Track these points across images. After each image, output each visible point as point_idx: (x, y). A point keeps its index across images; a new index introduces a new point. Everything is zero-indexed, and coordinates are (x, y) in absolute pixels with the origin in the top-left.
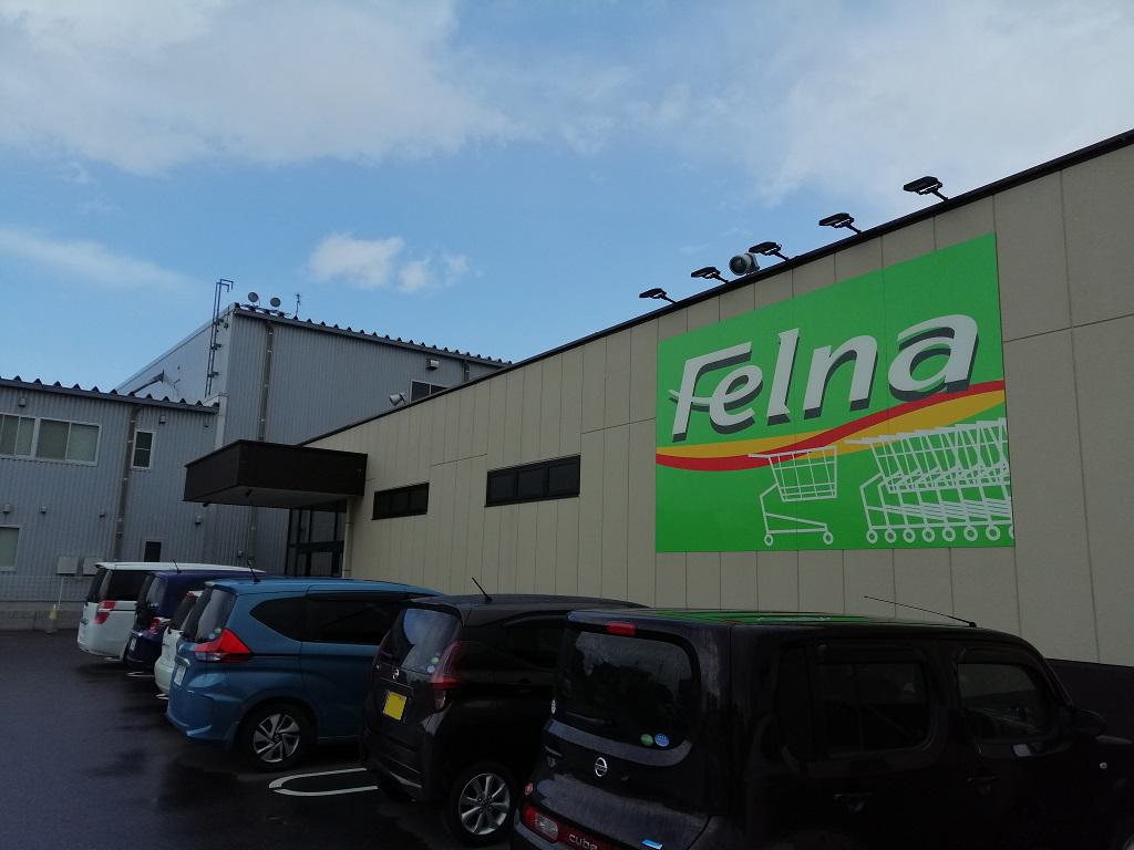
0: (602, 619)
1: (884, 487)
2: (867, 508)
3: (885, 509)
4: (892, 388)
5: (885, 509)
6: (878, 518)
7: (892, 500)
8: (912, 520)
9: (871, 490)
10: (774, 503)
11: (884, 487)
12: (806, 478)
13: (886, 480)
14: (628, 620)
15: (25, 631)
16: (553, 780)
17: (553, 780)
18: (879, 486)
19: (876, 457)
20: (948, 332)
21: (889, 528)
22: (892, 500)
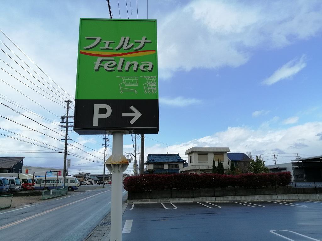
0: (35, 210)
1: (148, 85)
2: (121, 88)
3: (148, 88)
4: (105, 69)
5: (148, 88)
6: (147, 89)
7: (150, 87)
8: (153, 90)
9: (146, 85)
10: (123, 86)
11: (148, 85)
12: (131, 82)
13: (149, 84)
14: (71, 194)
15: (226, 71)
16: (257, 158)
17: (257, 158)
18: (147, 84)
19: (123, 80)
20: (108, 67)
21: (149, 91)
22: (150, 87)
